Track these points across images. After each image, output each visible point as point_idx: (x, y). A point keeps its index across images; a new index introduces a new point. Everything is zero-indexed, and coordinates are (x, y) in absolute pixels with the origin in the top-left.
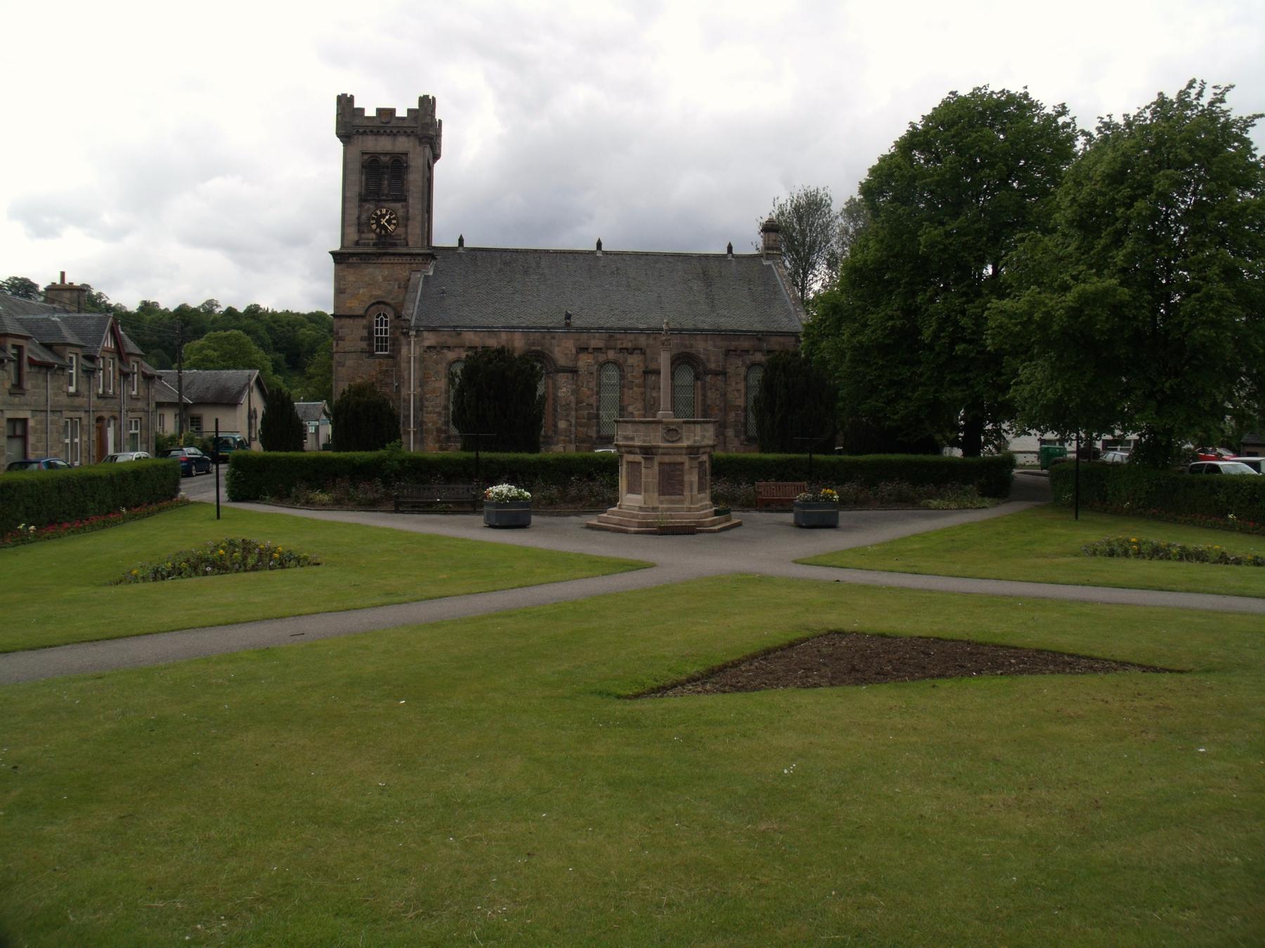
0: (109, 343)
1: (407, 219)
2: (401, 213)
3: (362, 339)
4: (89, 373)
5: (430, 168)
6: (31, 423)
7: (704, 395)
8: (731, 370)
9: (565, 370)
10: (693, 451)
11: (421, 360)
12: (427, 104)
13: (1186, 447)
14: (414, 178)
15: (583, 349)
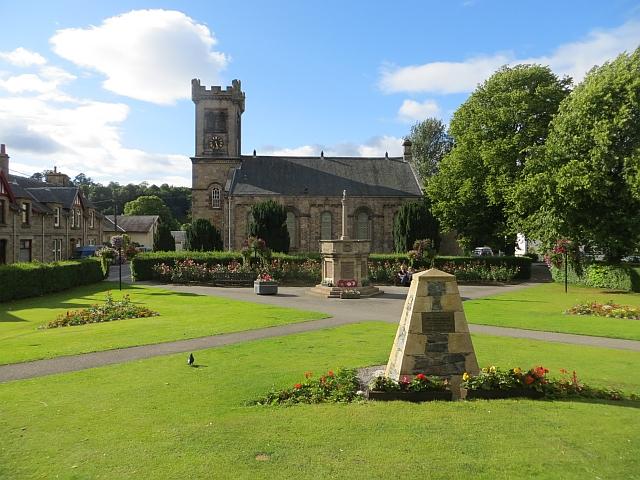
0: (77, 202)
1: (228, 142)
2: (224, 139)
3: (207, 201)
4: (66, 217)
5: (239, 117)
6: (33, 242)
7: (373, 228)
8: (386, 214)
9: (305, 215)
10: (358, 256)
11: (234, 211)
12: (237, 83)
13: (611, 183)
14: (231, 122)
15: (312, 205)
